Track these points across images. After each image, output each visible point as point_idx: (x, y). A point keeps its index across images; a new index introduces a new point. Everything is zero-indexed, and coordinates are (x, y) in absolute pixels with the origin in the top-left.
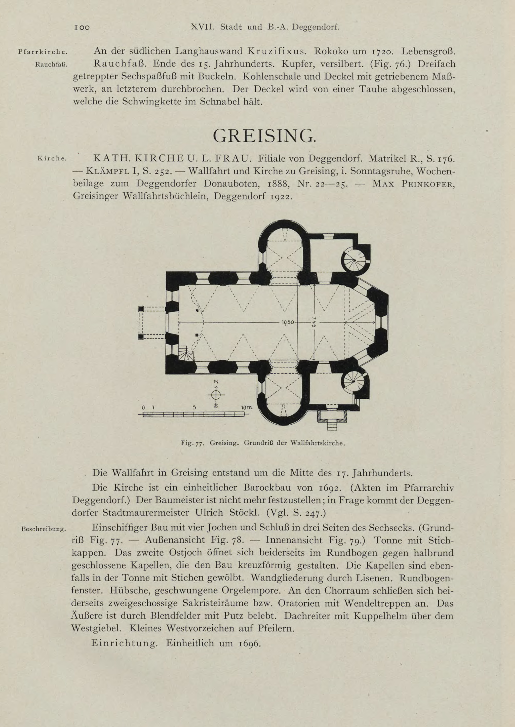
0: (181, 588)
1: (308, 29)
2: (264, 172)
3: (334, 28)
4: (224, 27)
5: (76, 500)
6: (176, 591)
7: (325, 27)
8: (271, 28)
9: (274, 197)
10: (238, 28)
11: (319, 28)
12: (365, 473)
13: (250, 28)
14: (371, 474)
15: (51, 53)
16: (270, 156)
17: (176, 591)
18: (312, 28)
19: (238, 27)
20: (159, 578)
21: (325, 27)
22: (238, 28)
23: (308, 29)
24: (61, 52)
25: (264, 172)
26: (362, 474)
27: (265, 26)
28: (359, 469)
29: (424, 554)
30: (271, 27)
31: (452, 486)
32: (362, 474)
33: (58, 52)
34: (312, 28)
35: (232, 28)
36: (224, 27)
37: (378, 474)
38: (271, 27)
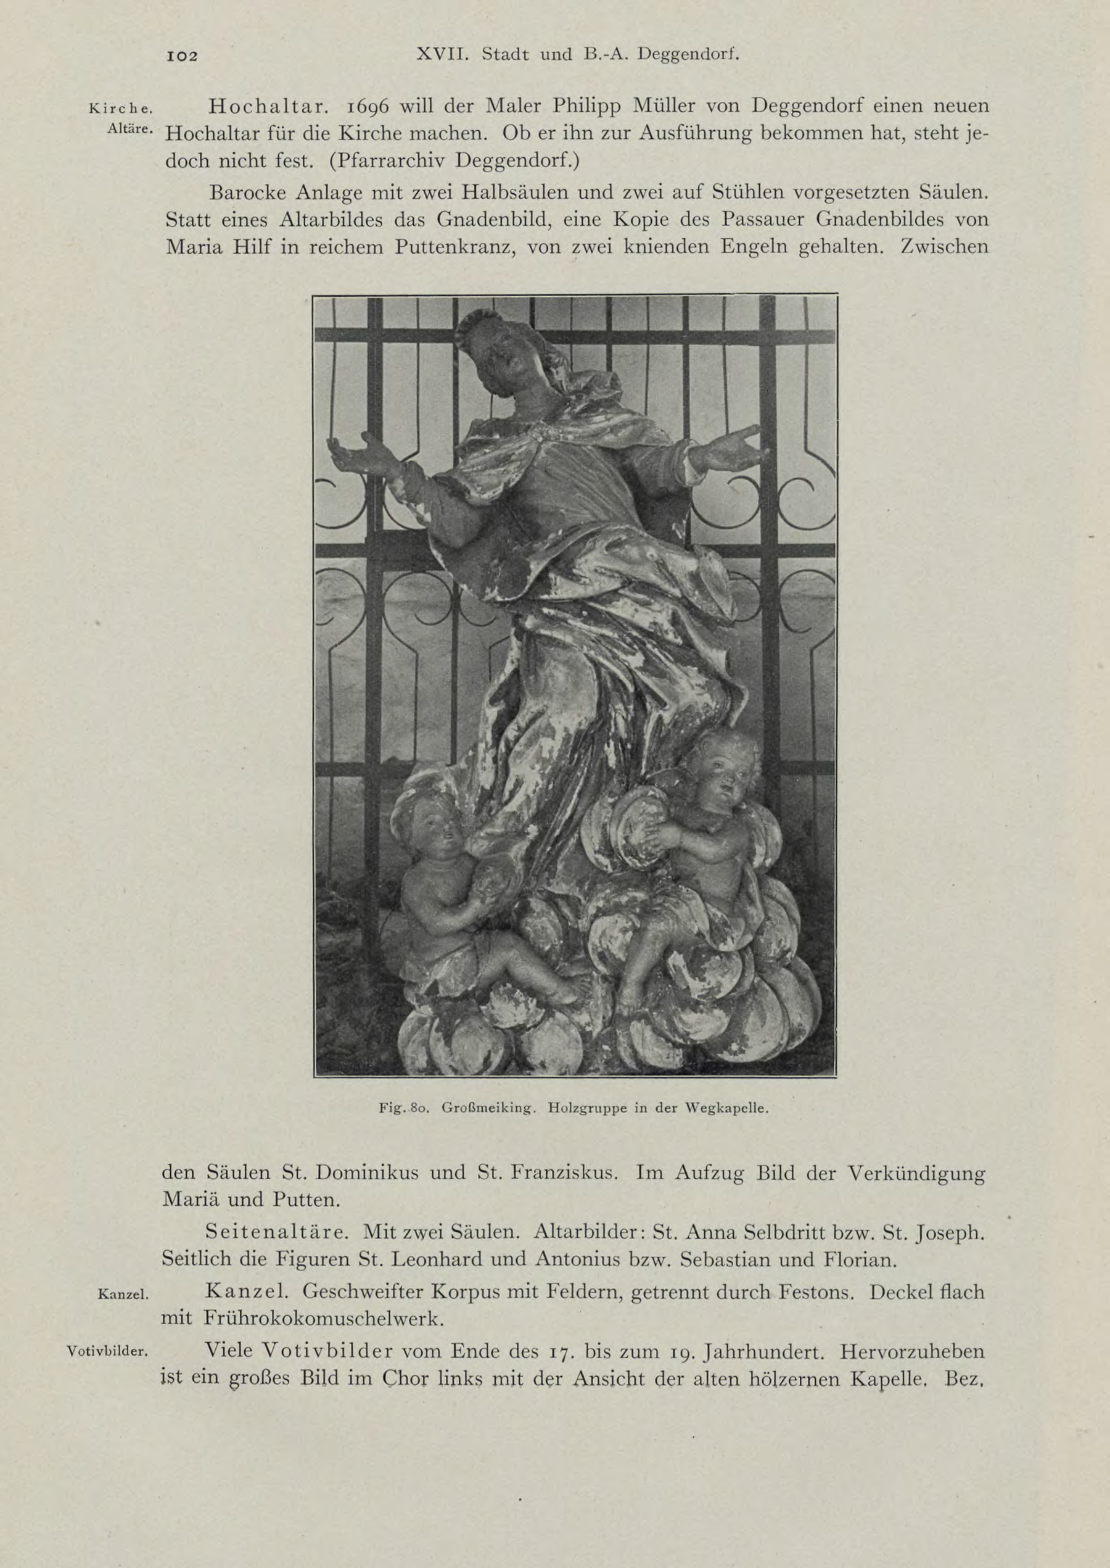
0: (364, 1287)
1: (672, 57)
2: (362, 135)
3: (727, 55)
4: (489, 54)
5: (761, 105)
6: (353, 1293)
7: (709, 55)
8: (591, 56)
9: (678, 1353)
10: (522, 56)
11: (694, 55)
12: (731, 1352)
13: (545, 56)
14: (744, 1354)
15: (116, 110)
16: (591, 100)
17: (353, 1293)
18: (679, 57)
19: (521, 55)
20: (356, 1174)
21: (709, 55)
22: (522, 56)
23: (672, 57)
24: (139, 109)
25: (362, 135)
26: (724, 1354)
27: (579, 53)
28: (718, 1344)
29: (490, 194)
30: (590, 53)
31: (440, 156)
32: (724, 1354)
33: (133, 109)
34: (679, 57)
35: (507, 57)
36: (489, 54)
37: (757, 1353)
38: (590, 53)
